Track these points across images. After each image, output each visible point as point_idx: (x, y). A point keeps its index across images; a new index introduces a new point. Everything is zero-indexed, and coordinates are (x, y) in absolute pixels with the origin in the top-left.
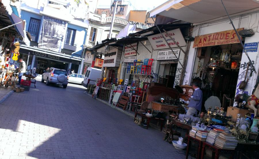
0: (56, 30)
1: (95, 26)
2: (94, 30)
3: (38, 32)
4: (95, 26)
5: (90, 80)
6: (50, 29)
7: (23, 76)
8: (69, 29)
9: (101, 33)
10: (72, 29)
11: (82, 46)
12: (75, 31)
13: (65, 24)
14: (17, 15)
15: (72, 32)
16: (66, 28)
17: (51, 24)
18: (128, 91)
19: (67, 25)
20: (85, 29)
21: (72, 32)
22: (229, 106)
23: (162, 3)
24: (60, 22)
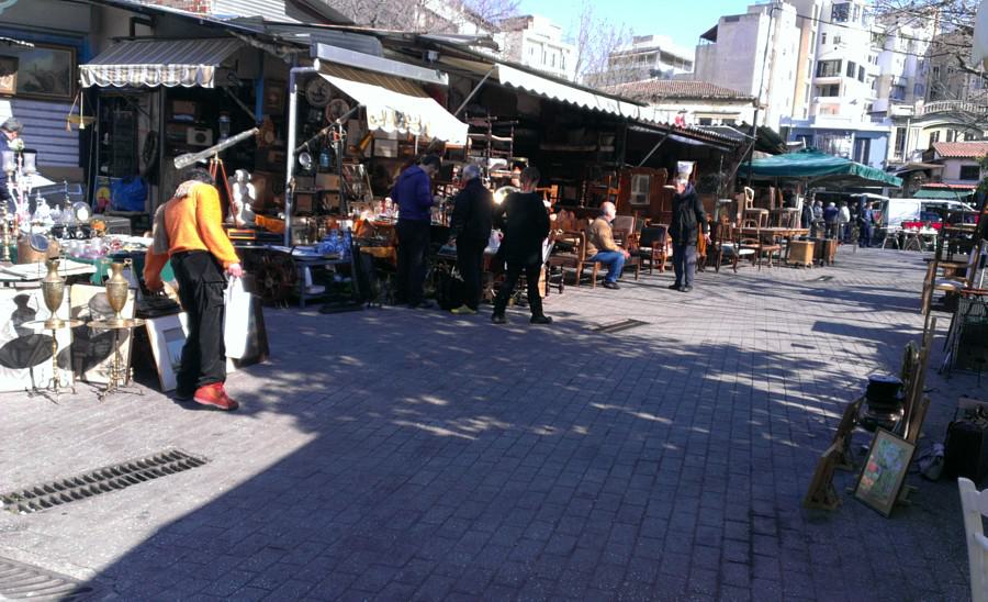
0: (837, 145)
1: (902, 126)
2: (902, 134)
3: (197, 209)
4: (902, 126)
5: (671, 287)
6: (827, 147)
7: (607, 215)
8: (858, 141)
9: (917, 133)
10: (862, 139)
11: (884, 163)
12: (868, 140)
13: (850, 134)
14: (154, 206)
15: (864, 142)
16: (853, 140)
17: (828, 140)
18: (46, 446)
19: (853, 135)
20: (886, 134)
21: (864, 142)
22: (470, 131)
23: (538, 78)
24: (842, 133)
